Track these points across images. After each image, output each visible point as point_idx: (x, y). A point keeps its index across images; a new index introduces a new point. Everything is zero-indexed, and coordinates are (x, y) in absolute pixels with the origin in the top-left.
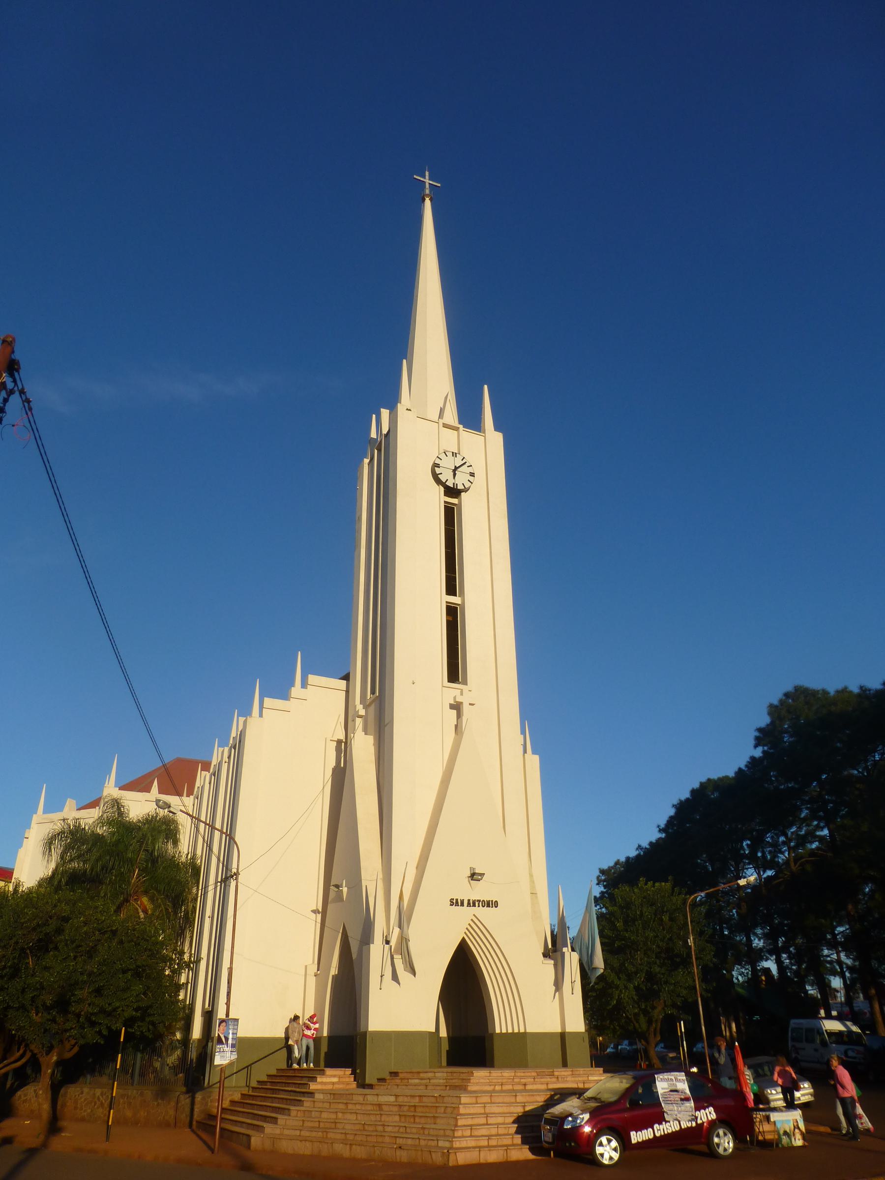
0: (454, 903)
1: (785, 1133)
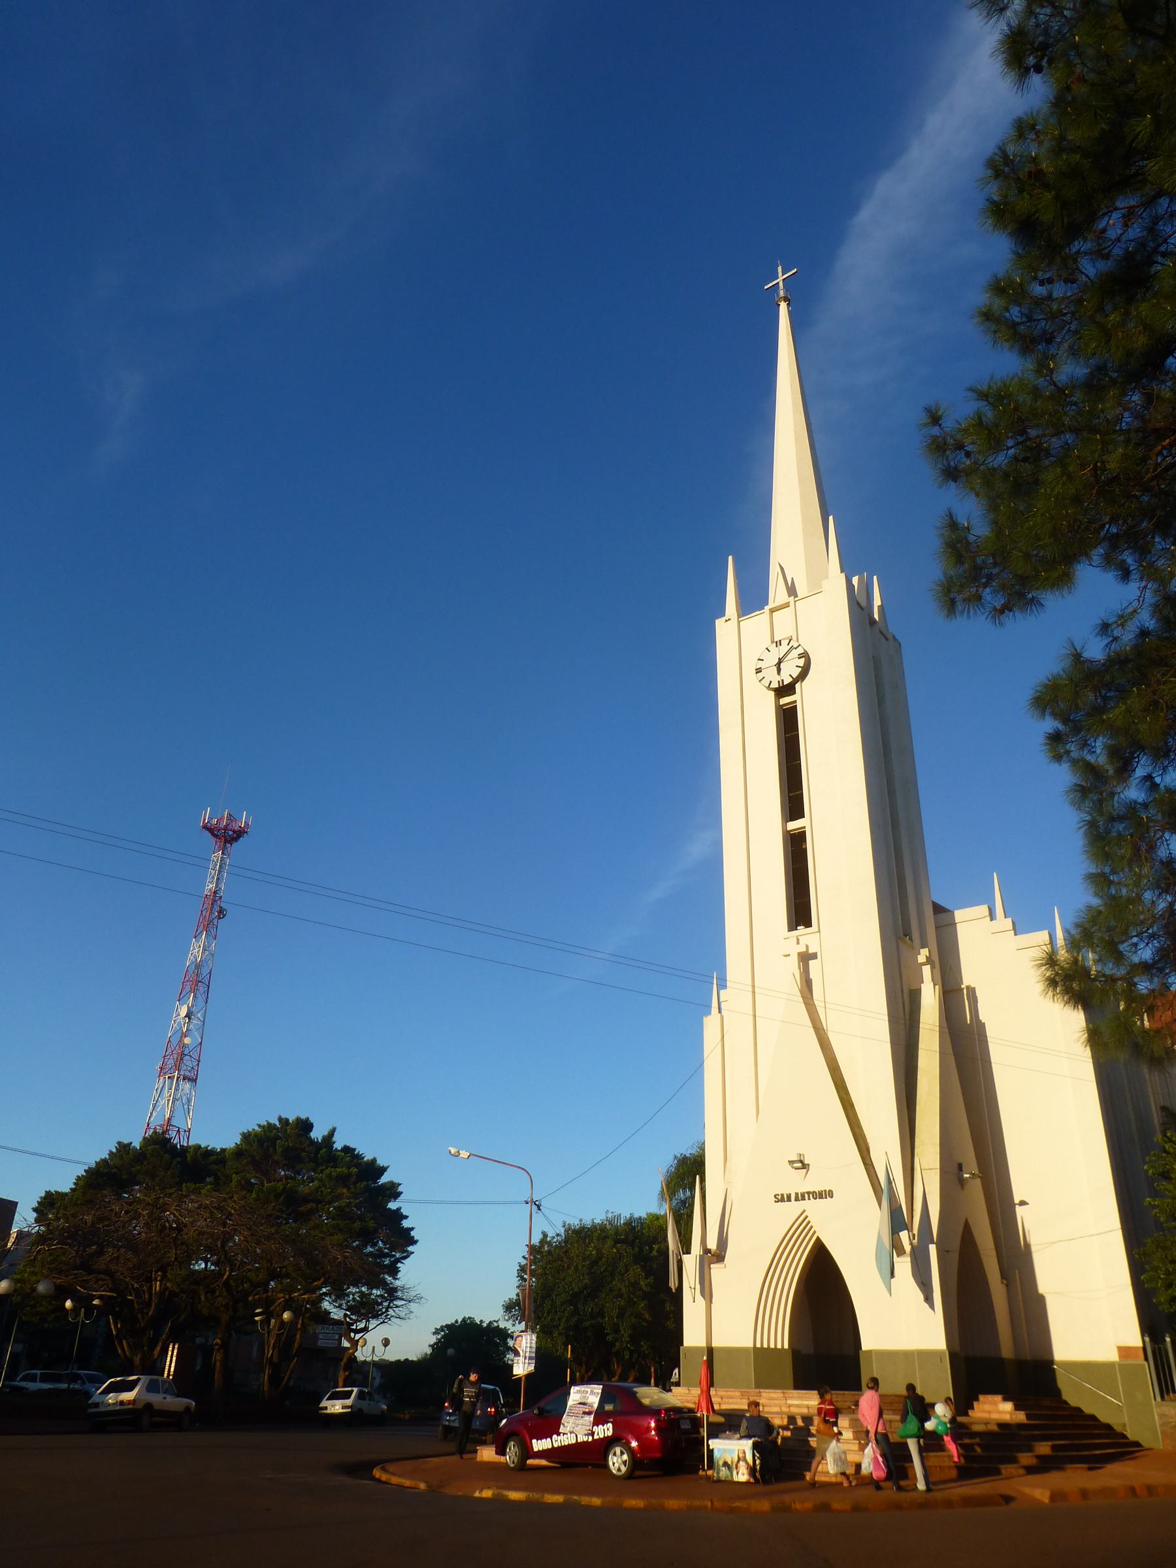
0: (781, 1199)
1: (726, 1464)
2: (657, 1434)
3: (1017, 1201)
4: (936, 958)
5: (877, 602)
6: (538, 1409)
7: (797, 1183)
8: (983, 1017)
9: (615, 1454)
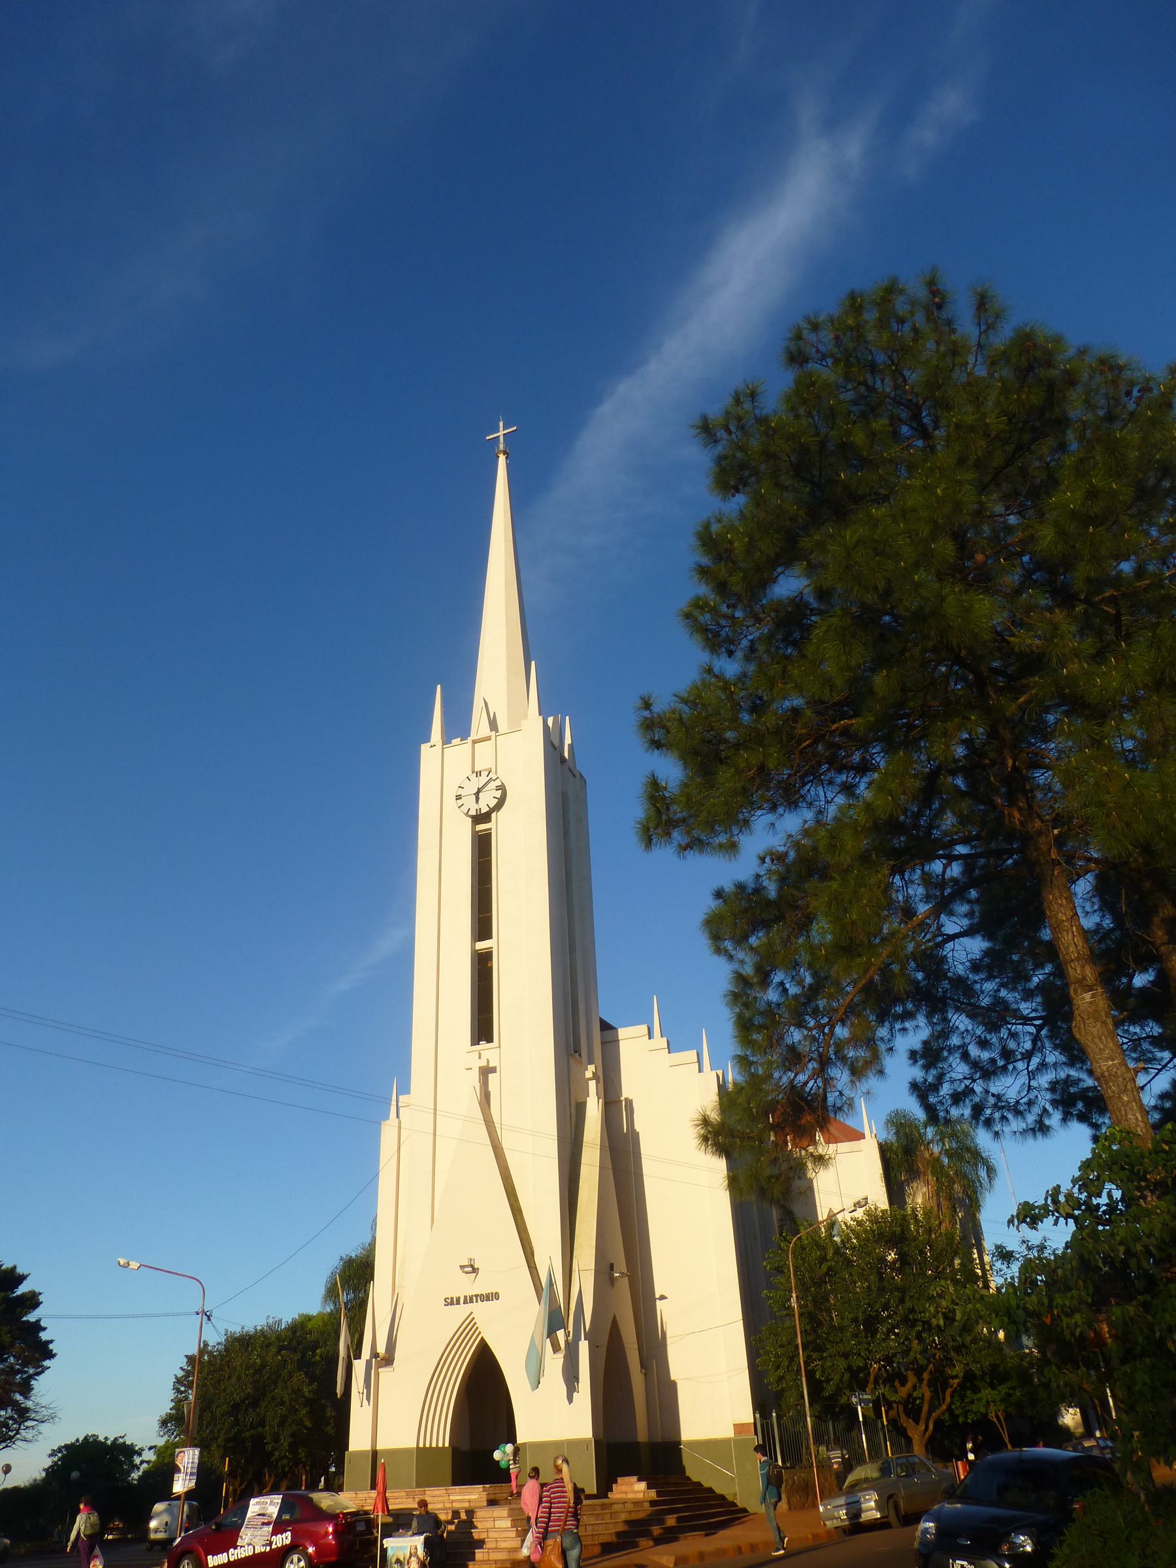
0: (451, 1302)
2: (334, 1538)
3: (657, 1296)
4: (600, 1074)
5: (568, 740)
6: (216, 1524)
7: (466, 1286)
8: (637, 1127)
9: (292, 1562)
